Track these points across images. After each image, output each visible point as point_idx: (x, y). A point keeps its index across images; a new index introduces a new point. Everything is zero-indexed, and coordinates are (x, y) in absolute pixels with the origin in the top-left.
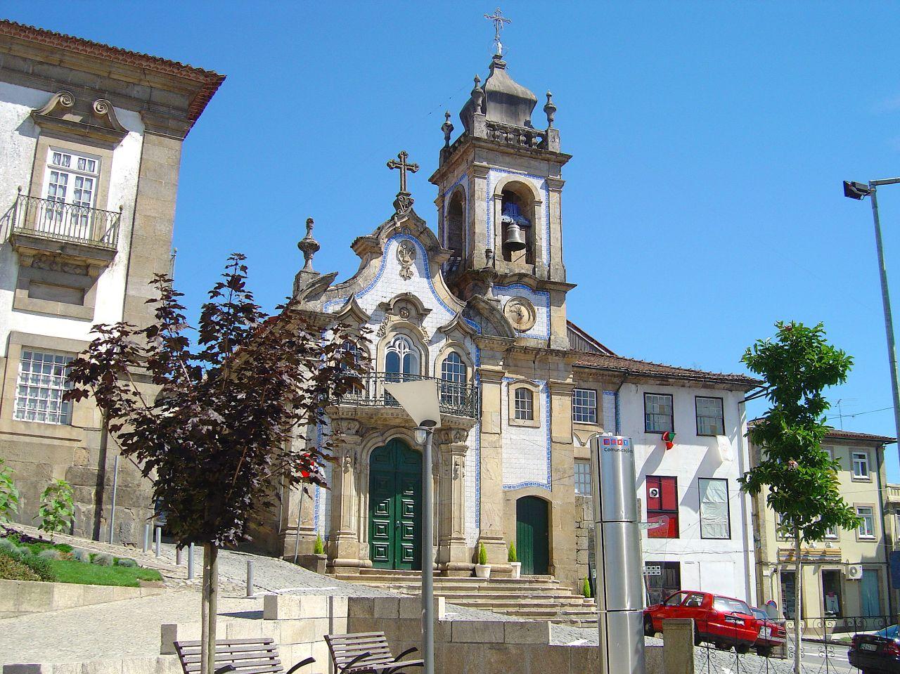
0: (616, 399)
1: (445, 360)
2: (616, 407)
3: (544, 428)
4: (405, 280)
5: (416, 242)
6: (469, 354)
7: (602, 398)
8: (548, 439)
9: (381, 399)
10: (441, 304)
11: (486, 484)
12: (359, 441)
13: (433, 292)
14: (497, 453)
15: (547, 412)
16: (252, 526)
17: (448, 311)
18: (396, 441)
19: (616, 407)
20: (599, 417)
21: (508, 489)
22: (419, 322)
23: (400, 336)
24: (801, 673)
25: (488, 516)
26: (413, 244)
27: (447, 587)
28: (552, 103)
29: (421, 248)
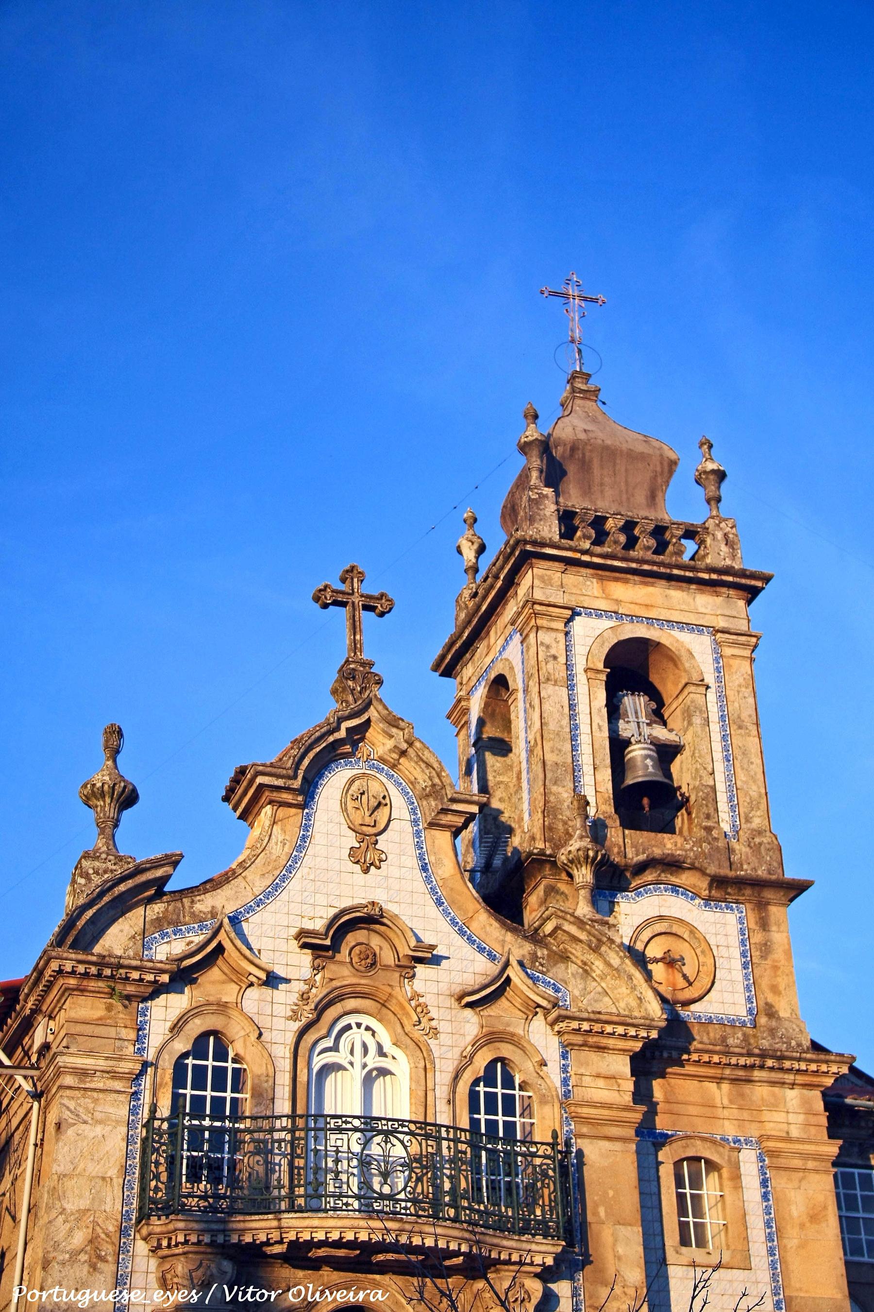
1: (476, 1082)
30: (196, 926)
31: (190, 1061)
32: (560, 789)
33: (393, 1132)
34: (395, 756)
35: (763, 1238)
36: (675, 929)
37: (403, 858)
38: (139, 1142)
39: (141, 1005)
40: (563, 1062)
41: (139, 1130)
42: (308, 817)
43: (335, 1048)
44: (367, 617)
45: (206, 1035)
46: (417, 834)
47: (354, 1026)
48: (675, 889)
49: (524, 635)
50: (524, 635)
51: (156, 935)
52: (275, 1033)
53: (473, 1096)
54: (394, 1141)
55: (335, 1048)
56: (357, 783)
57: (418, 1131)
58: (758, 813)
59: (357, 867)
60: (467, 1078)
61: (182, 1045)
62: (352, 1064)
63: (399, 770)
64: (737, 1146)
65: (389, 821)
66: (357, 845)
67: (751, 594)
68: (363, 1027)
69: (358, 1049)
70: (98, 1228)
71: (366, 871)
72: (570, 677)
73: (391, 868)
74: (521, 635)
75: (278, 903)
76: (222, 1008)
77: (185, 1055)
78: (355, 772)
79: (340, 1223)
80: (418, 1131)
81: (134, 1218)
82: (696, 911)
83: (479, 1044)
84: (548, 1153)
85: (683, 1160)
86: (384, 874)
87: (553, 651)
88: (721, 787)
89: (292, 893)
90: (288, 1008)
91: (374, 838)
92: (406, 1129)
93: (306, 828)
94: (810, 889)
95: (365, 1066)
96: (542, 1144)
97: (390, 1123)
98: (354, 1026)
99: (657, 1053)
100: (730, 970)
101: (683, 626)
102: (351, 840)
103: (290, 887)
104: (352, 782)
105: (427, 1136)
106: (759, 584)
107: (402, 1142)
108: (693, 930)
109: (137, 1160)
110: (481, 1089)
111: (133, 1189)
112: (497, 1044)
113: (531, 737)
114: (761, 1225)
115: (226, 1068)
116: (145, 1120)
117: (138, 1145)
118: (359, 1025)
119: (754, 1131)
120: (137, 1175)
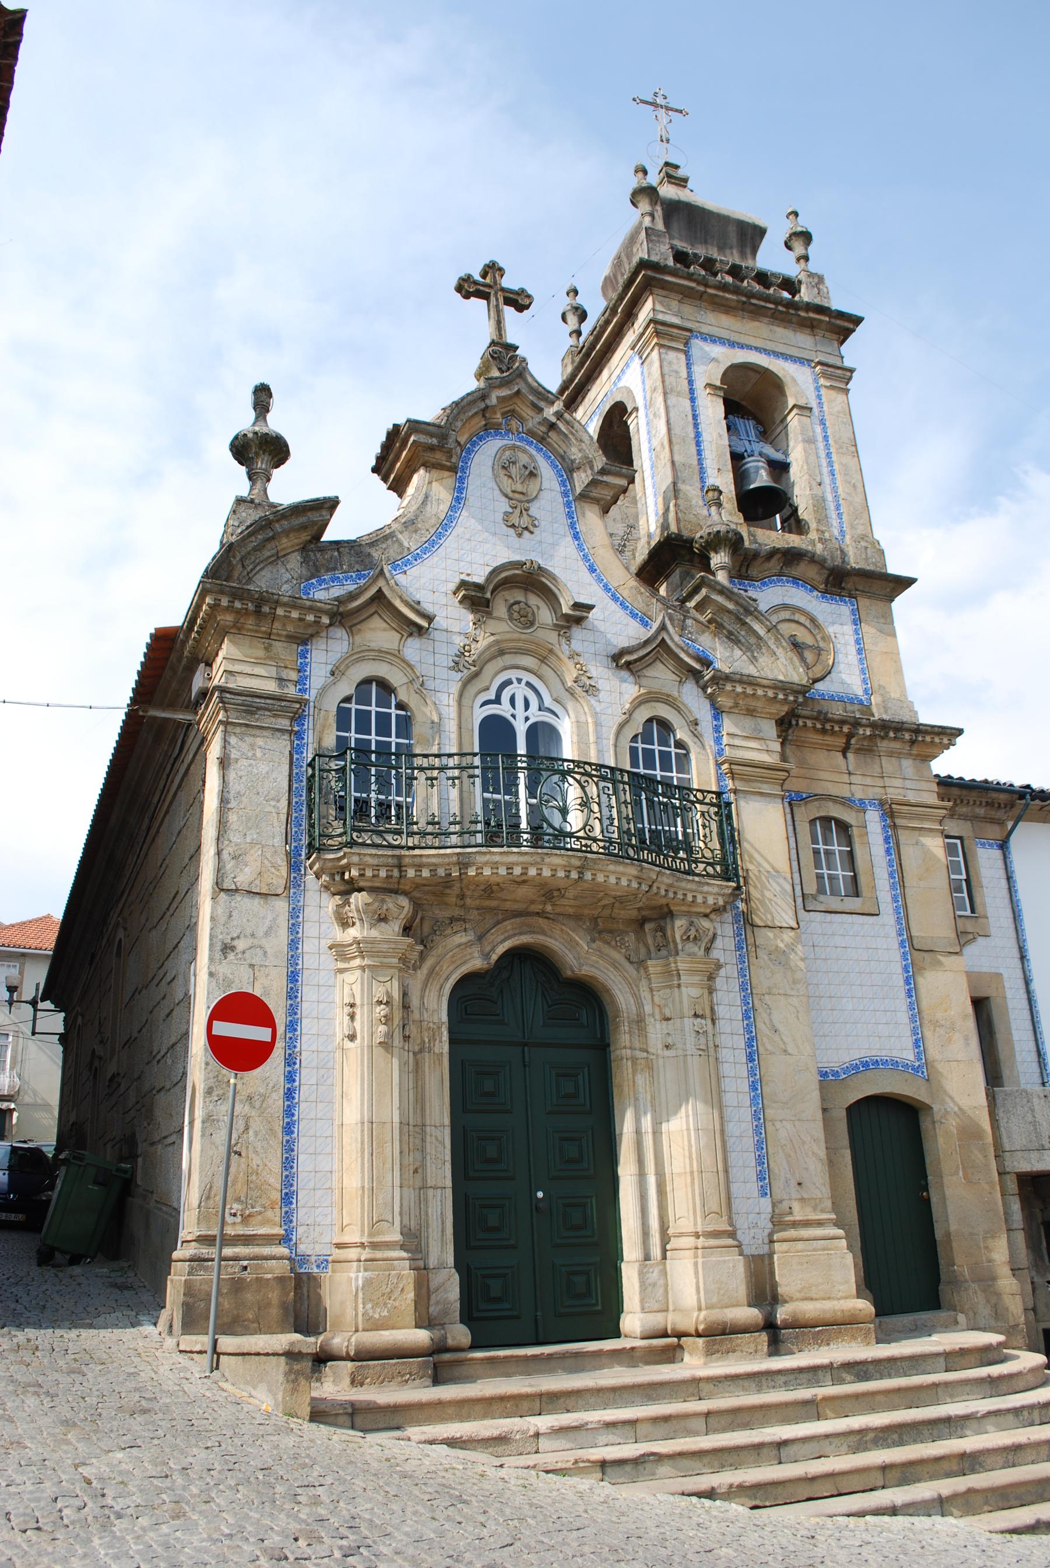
0: (1005, 858)
1: (634, 739)
2: (1009, 878)
3: (887, 906)
4: (520, 535)
5: (540, 450)
6: (696, 723)
7: (975, 855)
8: (902, 944)
9: (473, 828)
10: (614, 598)
11: (775, 1067)
12: (414, 956)
13: (592, 569)
14: (794, 982)
15: (891, 875)
16: (31, 1475)
17: (634, 616)
18: (518, 956)
19: (1009, 878)
20: (977, 900)
21: (827, 1080)
22: (563, 641)
23: (512, 674)
24: (17, 1565)
25: (788, 1156)
26: (531, 456)
27: (830, 1367)
28: (804, 223)
29: (553, 466)
30: (354, 575)
31: (353, 706)
32: (688, 488)
33: (569, 772)
34: (544, 429)
35: (888, 888)
36: (797, 617)
37: (556, 525)
38: (305, 780)
39: (300, 648)
40: (715, 723)
41: (304, 769)
42: (461, 480)
43: (497, 701)
44: (509, 311)
45: (367, 682)
46: (568, 505)
47: (515, 681)
48: (796, 580)
49: (644, 357)
50: (644, 357)
51: (313, 581)
52: (437, 681)
53: (633, 751)
54: (569, 779)
55: (497, 701)
56: (508, 453)
57: (594, 772)
58: (861, 521)
59: (511, 531)
60: (629, 733)
61: (346, 687)
62: (513, 716)
63: (549, 444)
64: (861, 807)
65: (541, 490)
66: (511, 510)
67: (844, 334)
68: (524, 682)
69: (520, 703)
70: (266, 861)
71: (520, 535)
72: (692, 391)
73: (544, 534)
74: (641, 357)
75: (436, 559)
76: (381, 655)
77: (347, 699)
78: (505, 442)
79: (521, 859)
80: (594, 772)
81: (303, 853)
82: (815, 602)
83: (639, 702)
84: (714, 801)
85: (814, 820)
86: (538, 538)
87: (675, 367)
88: (829, 497)
89: (449, 550)
90: (450, 659)
91: (527, 505)
92: (582, 770)
93: (460, 490)
94: (913, 586)
95: (527, 719)
96: (709, 792)
97: (566, 764)
98: (515, 681)
99: (794, 722)
100: (846, 655)
101: (786, 357)
102: (504, 505)
103: (446, 544)
104: (505, 448)
105: (604, 778)
106: (851, 326)
107: (578, 782)
108: (813, 620)
109: (304, 798)
110: (640, 746)
111: (301, 825)
112: (653, 704)
113: (655, 443)
114: (886, 876)
115: (390, 714)
116: (309, 760)
117: (304, 783)
118: (519, 681)
119: (876, 792)
120: (304, 813)
